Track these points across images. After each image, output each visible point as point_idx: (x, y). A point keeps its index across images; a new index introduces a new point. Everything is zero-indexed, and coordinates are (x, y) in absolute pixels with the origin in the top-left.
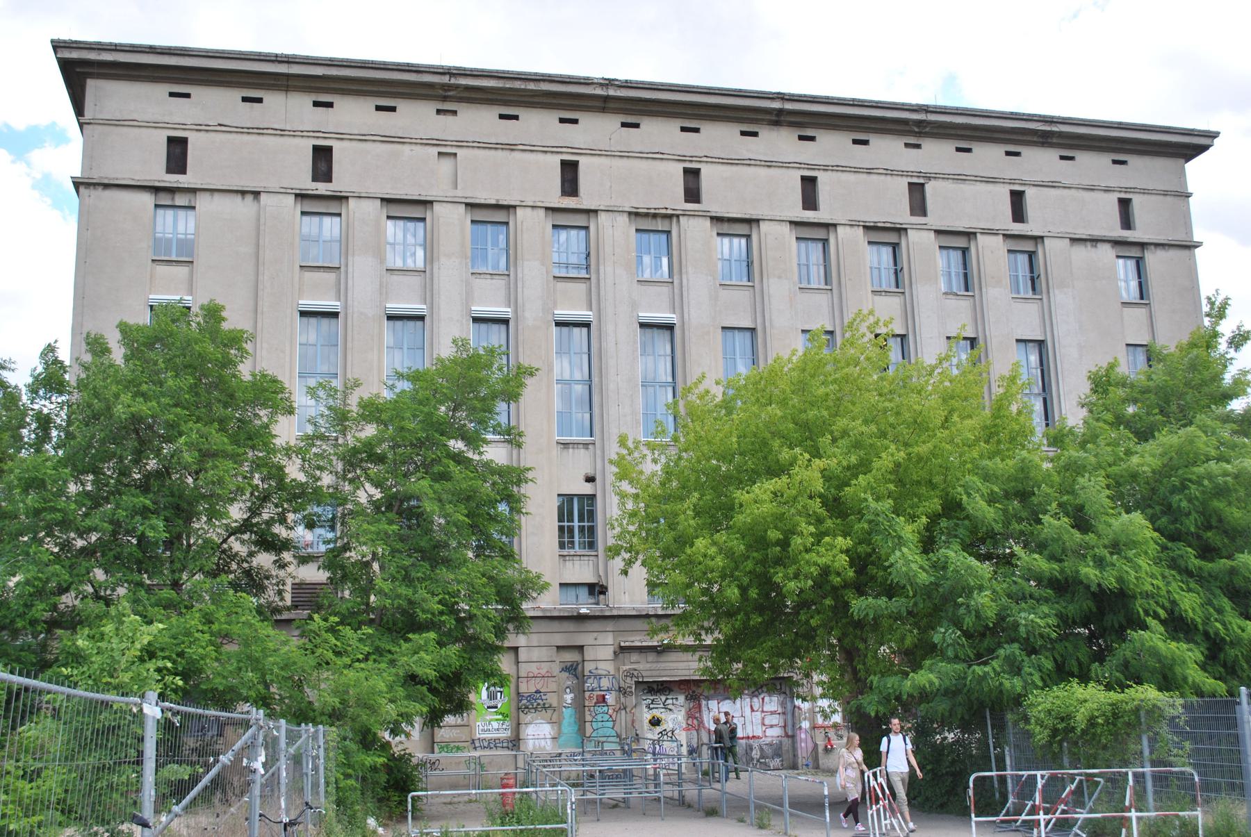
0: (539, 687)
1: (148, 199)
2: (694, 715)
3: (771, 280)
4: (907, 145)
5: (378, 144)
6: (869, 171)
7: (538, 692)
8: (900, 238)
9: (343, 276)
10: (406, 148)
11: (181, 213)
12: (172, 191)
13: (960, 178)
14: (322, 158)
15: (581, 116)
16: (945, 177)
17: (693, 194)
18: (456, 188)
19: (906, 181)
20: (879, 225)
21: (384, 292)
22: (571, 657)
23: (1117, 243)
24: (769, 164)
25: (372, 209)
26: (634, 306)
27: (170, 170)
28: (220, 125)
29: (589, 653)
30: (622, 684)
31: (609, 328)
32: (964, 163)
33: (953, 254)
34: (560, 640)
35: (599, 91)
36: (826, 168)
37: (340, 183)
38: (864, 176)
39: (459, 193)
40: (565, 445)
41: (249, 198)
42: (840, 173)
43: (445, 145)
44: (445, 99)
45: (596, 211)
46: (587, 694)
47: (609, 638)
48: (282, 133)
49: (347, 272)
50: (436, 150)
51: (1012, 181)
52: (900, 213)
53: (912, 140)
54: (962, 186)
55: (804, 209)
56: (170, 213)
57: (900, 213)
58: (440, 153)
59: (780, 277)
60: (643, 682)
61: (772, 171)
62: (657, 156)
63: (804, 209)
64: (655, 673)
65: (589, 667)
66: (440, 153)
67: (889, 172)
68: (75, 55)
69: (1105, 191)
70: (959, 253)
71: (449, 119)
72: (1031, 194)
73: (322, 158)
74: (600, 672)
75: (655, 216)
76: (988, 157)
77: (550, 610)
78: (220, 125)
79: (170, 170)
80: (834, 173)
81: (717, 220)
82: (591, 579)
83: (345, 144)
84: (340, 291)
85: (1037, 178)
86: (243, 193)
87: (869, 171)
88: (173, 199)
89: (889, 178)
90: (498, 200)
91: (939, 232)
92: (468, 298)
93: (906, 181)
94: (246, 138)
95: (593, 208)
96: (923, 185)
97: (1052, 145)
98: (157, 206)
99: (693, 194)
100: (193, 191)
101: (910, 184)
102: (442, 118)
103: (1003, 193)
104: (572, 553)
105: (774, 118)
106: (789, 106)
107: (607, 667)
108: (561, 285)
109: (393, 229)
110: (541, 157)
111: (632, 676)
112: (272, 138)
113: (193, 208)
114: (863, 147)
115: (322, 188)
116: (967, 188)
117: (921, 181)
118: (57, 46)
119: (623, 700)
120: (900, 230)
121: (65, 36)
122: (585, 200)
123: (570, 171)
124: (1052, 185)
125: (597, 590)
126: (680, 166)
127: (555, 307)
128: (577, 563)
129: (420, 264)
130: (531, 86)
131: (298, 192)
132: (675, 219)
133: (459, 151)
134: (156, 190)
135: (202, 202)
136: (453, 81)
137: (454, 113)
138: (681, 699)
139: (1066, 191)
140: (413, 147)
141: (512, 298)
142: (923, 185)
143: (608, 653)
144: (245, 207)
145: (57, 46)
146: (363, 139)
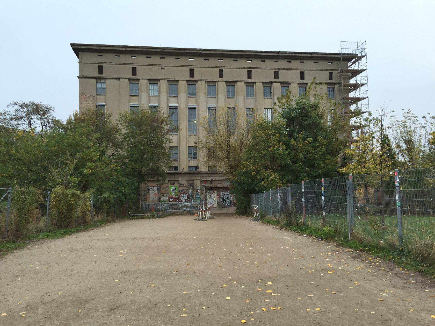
0: (183, 189)
1: (94, 81)
2: (219, 195)
3: (239, 96)
4: (275, 61)
5: (147, 66)
6: (264, 69)
7: (183, 190)
8: (196, 83)
9: (139, 98)
10: (153, 67)
11: (103, 83)
12: (100, 78)
13: (287, 69)
14: (134, 71)
15: (305, 61)
16: (284, 69)
17: (221, 76)
18: (165, 76)
19: (274, 70)
20: (266, 82)
21: (149, 101)
22: (191, 182)
23: (96, 78)
24: (240, 68)
25: (145, 82)
26: (206, 103)
27: (99, 73)
28: (110, 62)
29: (195, 182)
30: (202, 188)
31: (200, 108)
32: (290, 65)
33: (302, 88)
34: (188, 179)
35: (198, 52)
36: (254, 68)
37: (138, 76)
38: (263, 70)
39: (166, 77)
40: (190, 135)
41: (117, 80)
42: (257, 69)
43: (133, 65)
44: (162, 55)
45: (197, 81)
46: (194, 190)
47: (199, 178)
48: (125, 64)
49: (140, 97)
50: (160, 67)
51: (301, 69)
52: (272, 79)
53: (276, 60)
54: (288, 71)
55: (248, 78)
56: (100, 83)
57: (272, 79)
58: (161, 68)
59: (241, 95)
60: (207, 188)
61: (241, 69)
62: (212, 67)
63: (248, 78)
64: (223, 186)
65: (195, 184)
66: (161, 68)
67: (270, 69)
68: (76, 47)
69: (326, 71)
70: (304, 88)
71: (164, 59)
72: (306, 72)
73: (134, 71)
74: (197, 185)
75: (212, 82)
76: (296, 64)
77: (186, 172)
78: (110, 62)
79: (99, 73)
80: (256, 69)
81: (226, 82)
82: (196, 165)
83: (140, 66)
84: (139, 101)
85: (308, 68)
86: (116, 79)
87: (264, 69)
88: (100, 80)
89: (269, 70)
90: (175, 79)
91: (281, 83)
92: (168, 102)
93: (274, 70)
94: (116, 65)
95: (197, 80)
96: (278, 71)
97: (312, 60)
98: (97, 82)
99: (221, 76)
100: (105, 78)
101: (301, 72)
102: (162, 60)
103: (299, 72)
104: (191, 159)
105: (241, 56)
106: (244, 53)
107: (199, 184)
108: (190, 99)
109: (151, 87)
110: (185, 68)
111: (204, 186)
112: (122, 65)
113: (105, 82)
114: (276, 63)
115: (191, 79)
116: (289, 72)
117: (278, 70)
118: (72, 45)
119: (202, 191)
120: (272, 83)
121: (73, 43)
122: (195, 79)
123: (249, 73)
124: (312, 70)
125: (197, 167)
126: (218, 69)
127: (188, 104)
128: (193, 162)
129: (157, 95)
130: (182, 51)
131: (225, 81)
132: (216, 82)
133: (166, 68)
134: (96, 78)
135: (107, 81)
136: (163, 51)
137: (165, 58)
138: (216, 192)
139: (315, 71)
140: (155, 67)
141: (178, 102)
142: (278, 71)
143: (199, 181)
144: (117, 82)
145: (72, 45)
146: (143, 65)
